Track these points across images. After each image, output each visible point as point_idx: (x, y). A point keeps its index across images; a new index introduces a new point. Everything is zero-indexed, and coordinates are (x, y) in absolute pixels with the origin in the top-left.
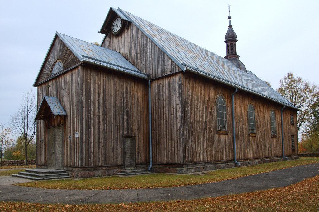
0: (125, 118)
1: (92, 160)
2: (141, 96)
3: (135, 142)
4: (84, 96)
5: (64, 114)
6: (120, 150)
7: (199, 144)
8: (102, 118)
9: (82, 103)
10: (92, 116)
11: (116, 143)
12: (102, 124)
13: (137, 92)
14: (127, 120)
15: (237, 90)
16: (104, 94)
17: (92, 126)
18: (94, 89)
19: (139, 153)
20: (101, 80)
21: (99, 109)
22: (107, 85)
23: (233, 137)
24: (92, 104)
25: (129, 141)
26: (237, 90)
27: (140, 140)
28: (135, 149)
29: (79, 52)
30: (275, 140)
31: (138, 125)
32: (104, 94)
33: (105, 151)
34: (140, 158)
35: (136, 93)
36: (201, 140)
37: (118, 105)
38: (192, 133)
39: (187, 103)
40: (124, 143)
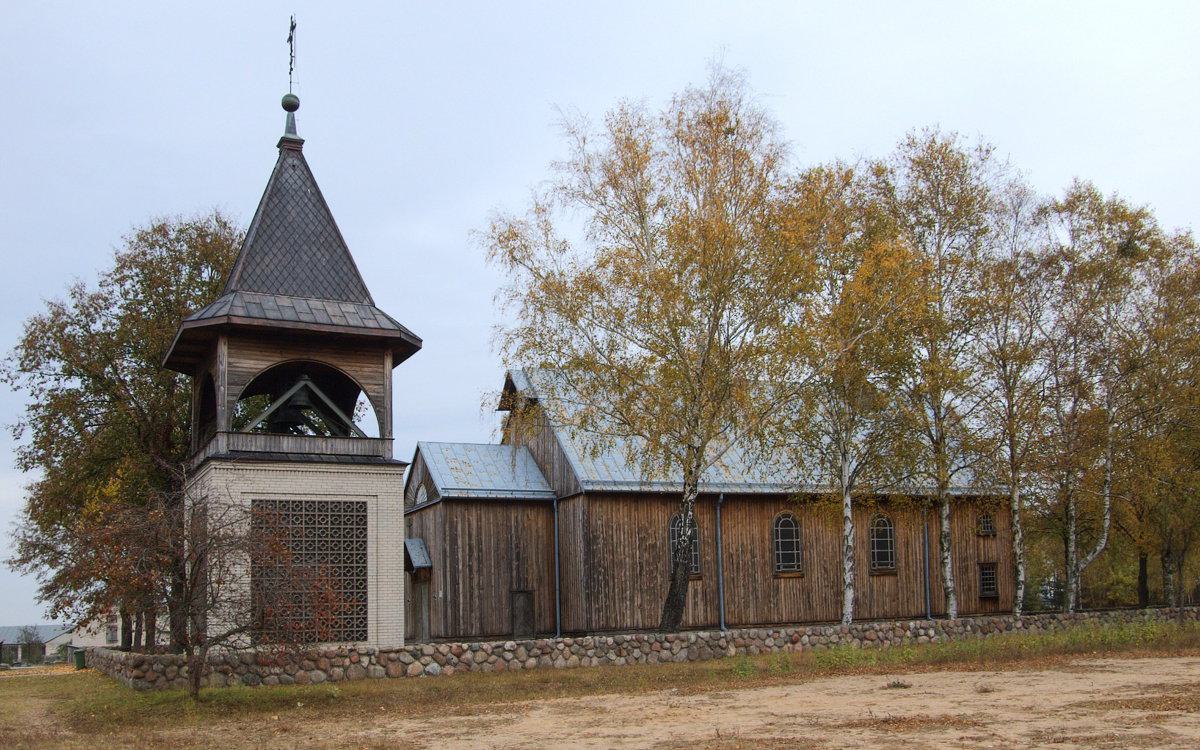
0: (515, 563)
1: (462, 627)
2: (545, 525)
3: (533, 600)
4: (448, 542)
5: (428, 564)
6: (506, 612)
7: (623, 599)
8: (475, 568)
9: (445, 551)
10: (460, 567)
11: (500, 601)
12: (476, 576)
13: (536, 521)
14: (518, 567)
15: (722, 497)
16: (479, 534)
17: (461, 582)
18: (463, 530)
19: (540, 616)
20: (473, 515)
21: (470, 556)
22: (483, 519)
23: (718, 584)
24: (460, 550)
25: (522, 598)
26: (722, 497)
27: (542, 597)
28: (533, 611)
29: (447, 481)
30: (888, 581)
31: (539, 572)
32: (479, 534)
33: (481, 614)
34: (543, 624)
35: (533, 525)
36: (628, 592)
37: (502, 546)
38: (607, 584)
39: (596, 538)
40: (512, 602)
